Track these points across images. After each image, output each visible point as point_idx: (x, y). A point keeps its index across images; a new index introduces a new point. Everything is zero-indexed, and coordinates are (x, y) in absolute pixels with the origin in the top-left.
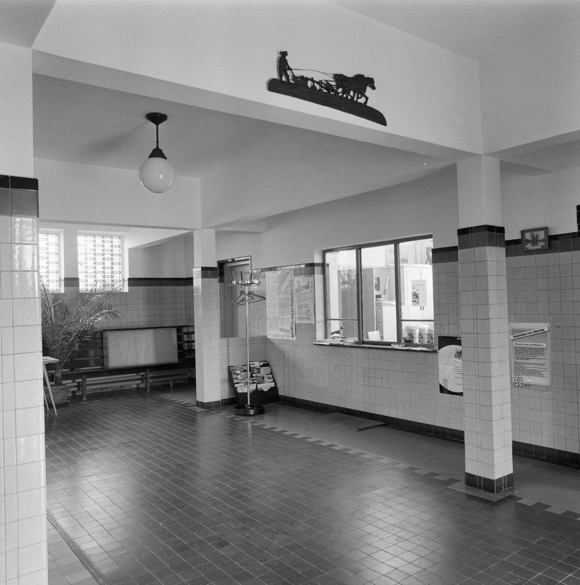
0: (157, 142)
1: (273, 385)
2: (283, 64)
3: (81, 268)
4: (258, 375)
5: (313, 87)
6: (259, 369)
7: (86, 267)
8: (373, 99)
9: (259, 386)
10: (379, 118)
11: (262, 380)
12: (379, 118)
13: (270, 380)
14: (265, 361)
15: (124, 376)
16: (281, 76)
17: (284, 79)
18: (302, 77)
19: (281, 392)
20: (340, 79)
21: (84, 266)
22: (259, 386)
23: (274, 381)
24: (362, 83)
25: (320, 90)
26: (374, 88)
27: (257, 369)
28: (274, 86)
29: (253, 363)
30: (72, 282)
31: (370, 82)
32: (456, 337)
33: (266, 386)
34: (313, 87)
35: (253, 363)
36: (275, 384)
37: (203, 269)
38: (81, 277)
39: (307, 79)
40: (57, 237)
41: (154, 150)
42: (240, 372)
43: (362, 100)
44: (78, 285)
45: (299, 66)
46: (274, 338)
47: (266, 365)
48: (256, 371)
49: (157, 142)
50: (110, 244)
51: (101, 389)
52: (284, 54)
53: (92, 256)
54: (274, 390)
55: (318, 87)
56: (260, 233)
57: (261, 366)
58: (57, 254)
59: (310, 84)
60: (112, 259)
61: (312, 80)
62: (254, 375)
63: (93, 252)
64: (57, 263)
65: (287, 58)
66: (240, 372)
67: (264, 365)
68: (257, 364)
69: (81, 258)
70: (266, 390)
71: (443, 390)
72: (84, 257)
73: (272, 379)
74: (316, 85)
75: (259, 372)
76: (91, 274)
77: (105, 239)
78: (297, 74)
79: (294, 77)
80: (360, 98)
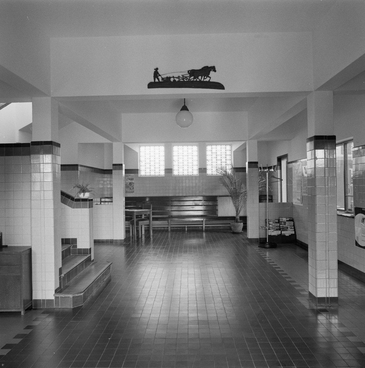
0: (185, 102)
1: (293, 232)
2: (156, 74)
3: (209, 163)
4: (284, 226)
5: (174, 80)
6: (285, 222)
7: (178, 163)
8: (214, 77)
9: (283, 232)
10: (219, 86)
11: (286, 229)
12: (219, 86)
13: (291, 230)
14: (291, 218)
15: (220, 221)
16: (155, 80)
17: (157, 80)
18: (167, 77)
19: (298, 238)
20: (193, 73)
21: (210, 162)
22: (283, 232)
23: (295, 230)
24: (206, 71)
25: (179, 81)
26: (215, 71)
27: (284, 222)
28: (151, 85)
29: (282, 218)
30: (169, 171)
31: (213, 69)
32: (362, 208)
33: (287, 233)
34: (174, 80)
35: (282, 218)
36: (295, 232)
37: (61, 165)
38: (209, 167)
39: (170, 78)
40: (230, 147)
41: (183, 107)
42: (272, 223)
43: (207, 79)
44: (206, 172)
45: (164, 73)
46: (296, 204)
47: (292, 220)
48: (283, 223)
49: (185, 102)
50: (213, 152)
51: (217, 227)
52: (157, 69)
53: (225, 156)
54: (295, 235)
55: (177, 80)
56: (291, 140)
57: (287, 221)
58: (230, 155)
59: (172, 80)
60: (192, 158)
61: (173, 77)
62: (281, 226)
63: (225, 154)
64: (230, 160)
65: (158, 71)
66: (272, 223)
67: (290, 220)
68: (284, 219)
69: (208, 158)
70: (287, 235)
71: (357, 244)
72: (227, 158)
73: (294, 229)
74: (175, 79)
75: (285, 224)
76: (214, 166)
77: (213, 147)
78: (164, 76)
79: (163, 79)
80: (206, 79)
